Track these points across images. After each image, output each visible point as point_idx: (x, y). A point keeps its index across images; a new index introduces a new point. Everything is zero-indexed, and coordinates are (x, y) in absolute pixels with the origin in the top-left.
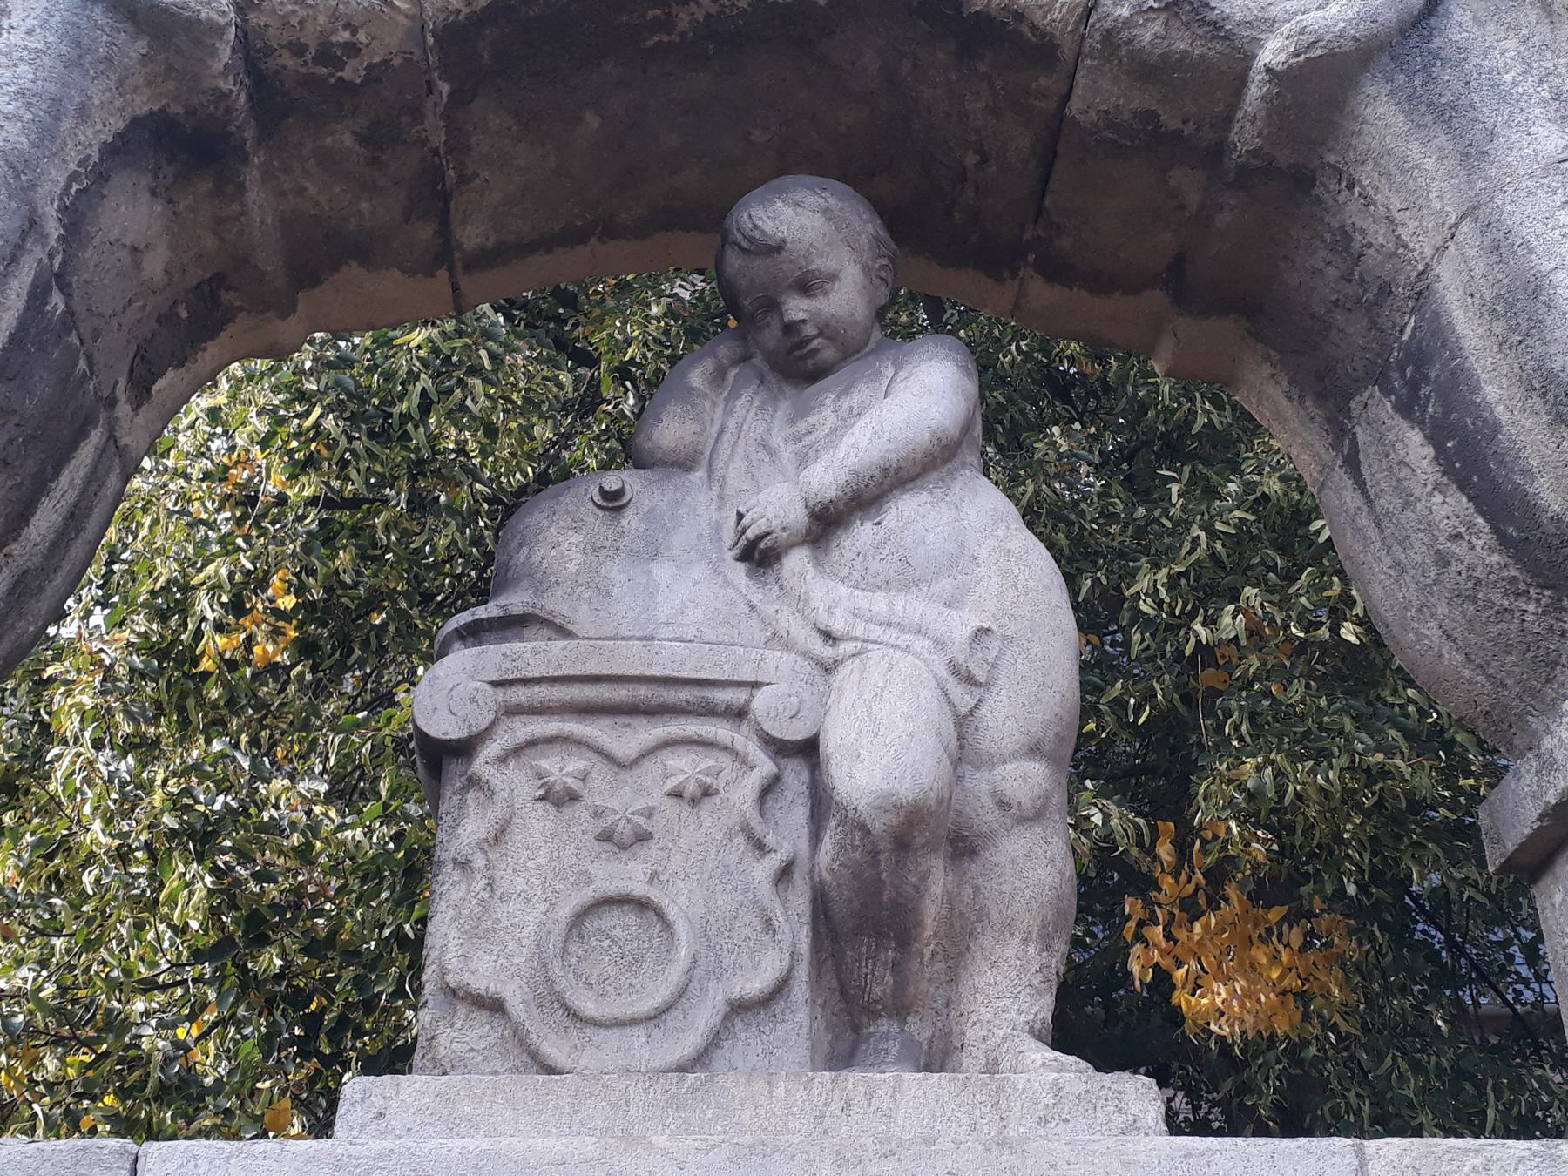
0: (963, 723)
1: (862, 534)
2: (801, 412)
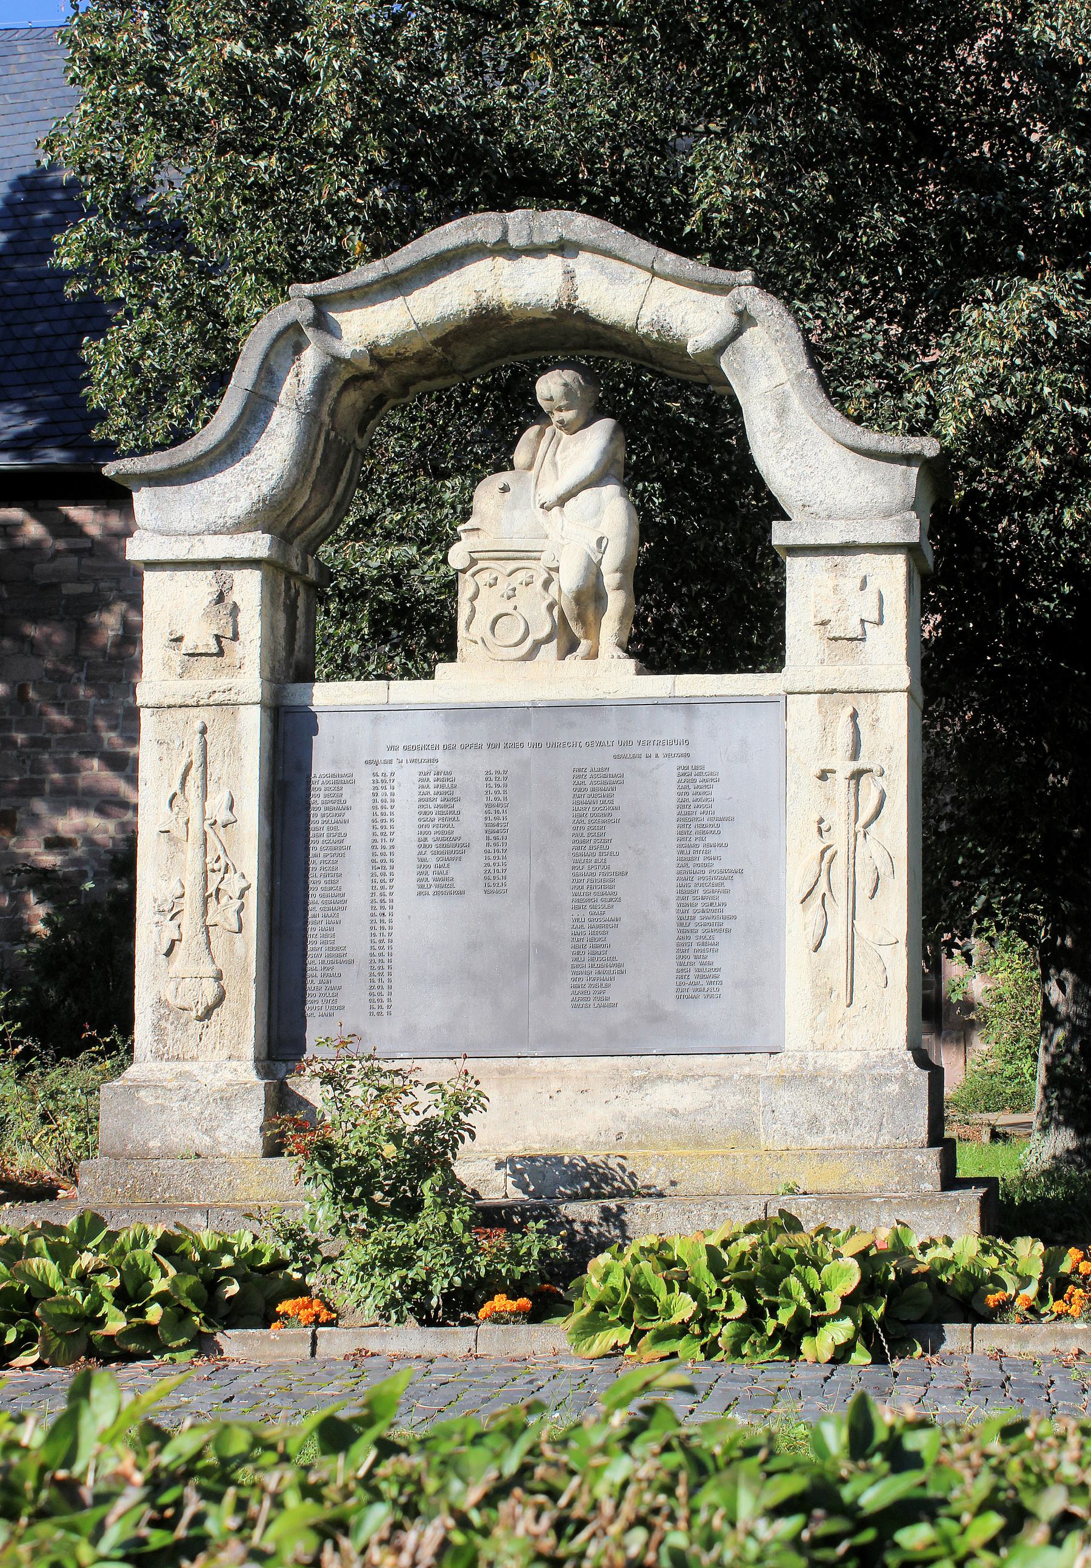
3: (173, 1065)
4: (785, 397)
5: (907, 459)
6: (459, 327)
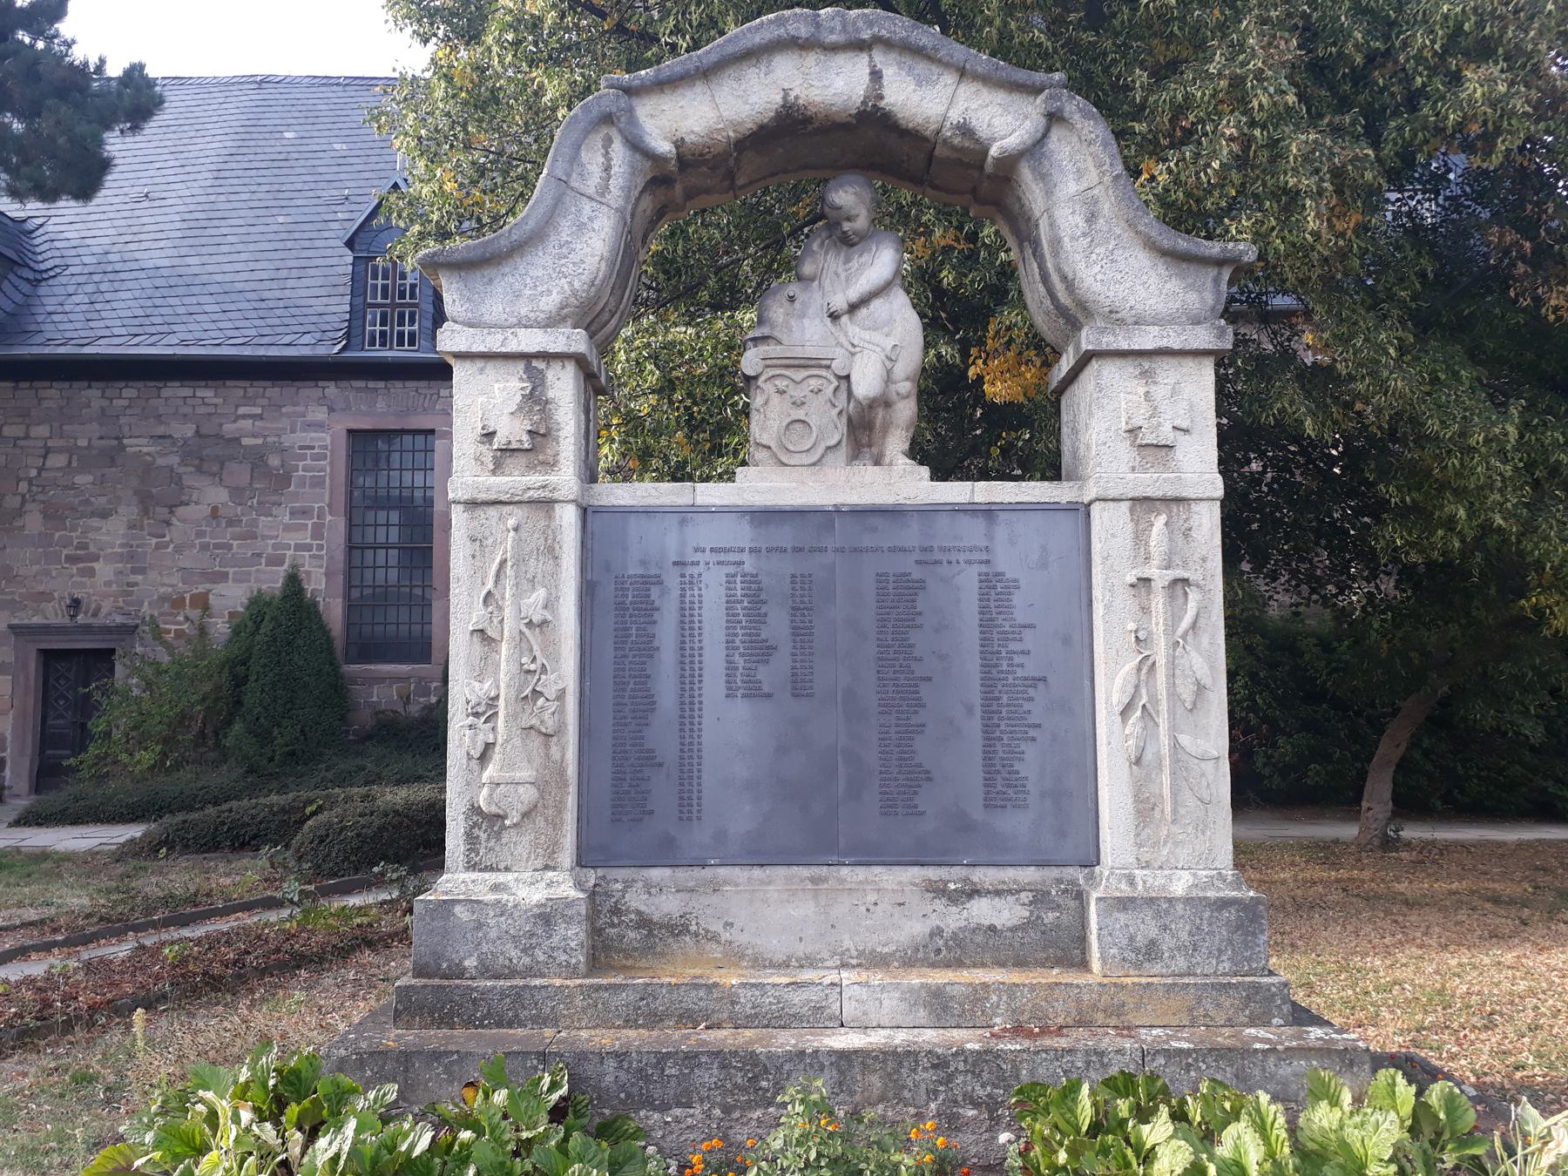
0: (889, 372)
1: (864, 312)
2: (847, 261)
3: (486, 875)
4: (1095, 201)
5: (1220, 263)
6: (762, 127)
